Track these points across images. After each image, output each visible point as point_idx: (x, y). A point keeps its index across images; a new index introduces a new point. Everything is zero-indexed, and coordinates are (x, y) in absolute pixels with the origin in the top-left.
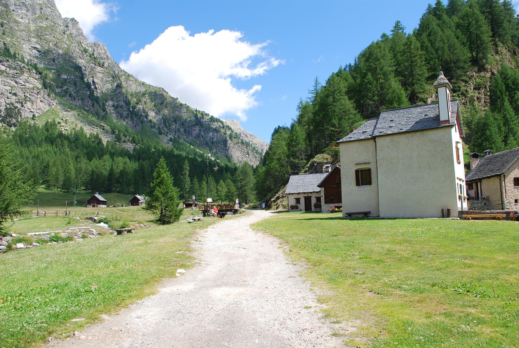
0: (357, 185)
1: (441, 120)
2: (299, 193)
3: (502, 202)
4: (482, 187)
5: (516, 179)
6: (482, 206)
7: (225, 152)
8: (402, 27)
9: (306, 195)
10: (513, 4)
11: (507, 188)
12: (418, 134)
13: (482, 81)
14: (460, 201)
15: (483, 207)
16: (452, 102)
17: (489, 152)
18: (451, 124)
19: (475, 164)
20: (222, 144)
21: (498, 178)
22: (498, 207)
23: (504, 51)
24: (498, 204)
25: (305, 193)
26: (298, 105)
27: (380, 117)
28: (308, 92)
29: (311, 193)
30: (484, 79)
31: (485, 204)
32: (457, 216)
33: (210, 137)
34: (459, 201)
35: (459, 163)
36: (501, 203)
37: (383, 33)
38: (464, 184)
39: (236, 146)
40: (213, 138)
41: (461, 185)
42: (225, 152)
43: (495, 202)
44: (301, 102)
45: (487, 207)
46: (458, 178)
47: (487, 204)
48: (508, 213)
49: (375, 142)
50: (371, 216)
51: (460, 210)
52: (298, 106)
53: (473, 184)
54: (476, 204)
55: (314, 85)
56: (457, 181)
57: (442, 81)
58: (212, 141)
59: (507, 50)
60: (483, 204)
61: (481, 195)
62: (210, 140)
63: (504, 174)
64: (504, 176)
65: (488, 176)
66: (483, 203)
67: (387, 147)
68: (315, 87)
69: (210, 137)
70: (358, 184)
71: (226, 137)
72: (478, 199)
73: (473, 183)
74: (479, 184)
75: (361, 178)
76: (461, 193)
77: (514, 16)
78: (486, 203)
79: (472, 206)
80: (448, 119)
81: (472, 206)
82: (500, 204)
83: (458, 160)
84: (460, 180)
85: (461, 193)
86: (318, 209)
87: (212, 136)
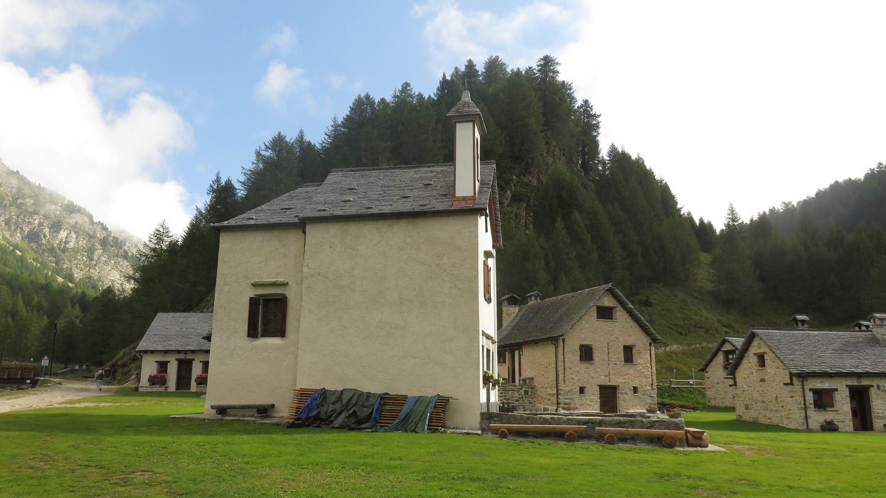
0: (248, 336)
1: (457, 195)
2: (166, 352)
3: (557, 390)
4: (522, 360)
5: (583, 349)
6: (520, 396)
7: (89, 271)
8: (412, 93)
9: (182, 356)
10: (573, 88)
11: (567, 365)
12: (404, 223)
13: (525, 190)
14: (486, 389)
15: (522, 398)
16: (483, 166)
17: (535, 296)
18: (478, 206)
19: (512, 311)
20: (84, 255)
21: (552, 343)
22: (549, 400)
23: (558, 153)
24: (549, 394)
25: (179, 352)
26: (212, 184)
27: (326, 181)
28: (241, 171)
29: (193, 352)
30: (528, 187)
31: (526, 392)
32: (478, 426)
33: (61, 240)
34: (484, 387)
35: (489, 300)
36: (555, 392)
37: (381, 98)
38: (494, 349)
39: (113, 262)
40: (66, 243)
41: (488, 351)
42: (89, 271)
43: (544, 390)
44: (218, 180)
45: (530, 399)
46: (484, 334)
47: (530, 393)
48: (592, 423)
49: (305, 233)
50: (275, 416)
51: (485, 410)
52: (211, 186)
53: (507, 353)
54: (510, 392)
55: (255, 162)
56: (483, 341)
57: (466, 109)
58: (65, 247)
59: (562, 153)
60: (523, 393)
61: (520, 375)
62: (60, 244)
63: (563, 337)
64: (564, 340)
65: (535, 338)
66: (522, 391)
67: (331, 247)
68: (255, 165)
69: (61, 240)
70: (253, 333)
71: (94, 242)
72: (514, 381)
73: (507, 351)
74: (517, 353)
75: (263, 317)
76: (488, 368)
77: (574, 106)
78: (528, 391)
79: (503, 395)
80: (472, 194)
81: (503, 395)
82: (554, 394)
83: (487, 294)
84: (489, 337)
85: (488, 368)
86: (157, 388)
87: (66, 238)
